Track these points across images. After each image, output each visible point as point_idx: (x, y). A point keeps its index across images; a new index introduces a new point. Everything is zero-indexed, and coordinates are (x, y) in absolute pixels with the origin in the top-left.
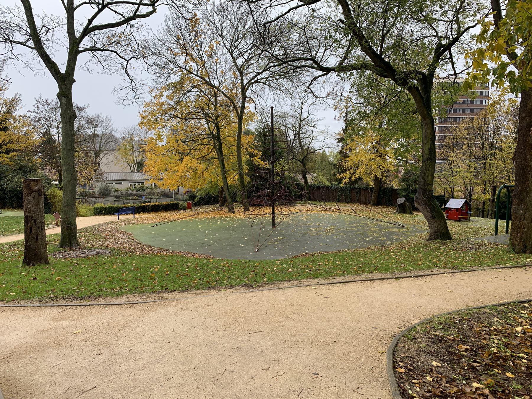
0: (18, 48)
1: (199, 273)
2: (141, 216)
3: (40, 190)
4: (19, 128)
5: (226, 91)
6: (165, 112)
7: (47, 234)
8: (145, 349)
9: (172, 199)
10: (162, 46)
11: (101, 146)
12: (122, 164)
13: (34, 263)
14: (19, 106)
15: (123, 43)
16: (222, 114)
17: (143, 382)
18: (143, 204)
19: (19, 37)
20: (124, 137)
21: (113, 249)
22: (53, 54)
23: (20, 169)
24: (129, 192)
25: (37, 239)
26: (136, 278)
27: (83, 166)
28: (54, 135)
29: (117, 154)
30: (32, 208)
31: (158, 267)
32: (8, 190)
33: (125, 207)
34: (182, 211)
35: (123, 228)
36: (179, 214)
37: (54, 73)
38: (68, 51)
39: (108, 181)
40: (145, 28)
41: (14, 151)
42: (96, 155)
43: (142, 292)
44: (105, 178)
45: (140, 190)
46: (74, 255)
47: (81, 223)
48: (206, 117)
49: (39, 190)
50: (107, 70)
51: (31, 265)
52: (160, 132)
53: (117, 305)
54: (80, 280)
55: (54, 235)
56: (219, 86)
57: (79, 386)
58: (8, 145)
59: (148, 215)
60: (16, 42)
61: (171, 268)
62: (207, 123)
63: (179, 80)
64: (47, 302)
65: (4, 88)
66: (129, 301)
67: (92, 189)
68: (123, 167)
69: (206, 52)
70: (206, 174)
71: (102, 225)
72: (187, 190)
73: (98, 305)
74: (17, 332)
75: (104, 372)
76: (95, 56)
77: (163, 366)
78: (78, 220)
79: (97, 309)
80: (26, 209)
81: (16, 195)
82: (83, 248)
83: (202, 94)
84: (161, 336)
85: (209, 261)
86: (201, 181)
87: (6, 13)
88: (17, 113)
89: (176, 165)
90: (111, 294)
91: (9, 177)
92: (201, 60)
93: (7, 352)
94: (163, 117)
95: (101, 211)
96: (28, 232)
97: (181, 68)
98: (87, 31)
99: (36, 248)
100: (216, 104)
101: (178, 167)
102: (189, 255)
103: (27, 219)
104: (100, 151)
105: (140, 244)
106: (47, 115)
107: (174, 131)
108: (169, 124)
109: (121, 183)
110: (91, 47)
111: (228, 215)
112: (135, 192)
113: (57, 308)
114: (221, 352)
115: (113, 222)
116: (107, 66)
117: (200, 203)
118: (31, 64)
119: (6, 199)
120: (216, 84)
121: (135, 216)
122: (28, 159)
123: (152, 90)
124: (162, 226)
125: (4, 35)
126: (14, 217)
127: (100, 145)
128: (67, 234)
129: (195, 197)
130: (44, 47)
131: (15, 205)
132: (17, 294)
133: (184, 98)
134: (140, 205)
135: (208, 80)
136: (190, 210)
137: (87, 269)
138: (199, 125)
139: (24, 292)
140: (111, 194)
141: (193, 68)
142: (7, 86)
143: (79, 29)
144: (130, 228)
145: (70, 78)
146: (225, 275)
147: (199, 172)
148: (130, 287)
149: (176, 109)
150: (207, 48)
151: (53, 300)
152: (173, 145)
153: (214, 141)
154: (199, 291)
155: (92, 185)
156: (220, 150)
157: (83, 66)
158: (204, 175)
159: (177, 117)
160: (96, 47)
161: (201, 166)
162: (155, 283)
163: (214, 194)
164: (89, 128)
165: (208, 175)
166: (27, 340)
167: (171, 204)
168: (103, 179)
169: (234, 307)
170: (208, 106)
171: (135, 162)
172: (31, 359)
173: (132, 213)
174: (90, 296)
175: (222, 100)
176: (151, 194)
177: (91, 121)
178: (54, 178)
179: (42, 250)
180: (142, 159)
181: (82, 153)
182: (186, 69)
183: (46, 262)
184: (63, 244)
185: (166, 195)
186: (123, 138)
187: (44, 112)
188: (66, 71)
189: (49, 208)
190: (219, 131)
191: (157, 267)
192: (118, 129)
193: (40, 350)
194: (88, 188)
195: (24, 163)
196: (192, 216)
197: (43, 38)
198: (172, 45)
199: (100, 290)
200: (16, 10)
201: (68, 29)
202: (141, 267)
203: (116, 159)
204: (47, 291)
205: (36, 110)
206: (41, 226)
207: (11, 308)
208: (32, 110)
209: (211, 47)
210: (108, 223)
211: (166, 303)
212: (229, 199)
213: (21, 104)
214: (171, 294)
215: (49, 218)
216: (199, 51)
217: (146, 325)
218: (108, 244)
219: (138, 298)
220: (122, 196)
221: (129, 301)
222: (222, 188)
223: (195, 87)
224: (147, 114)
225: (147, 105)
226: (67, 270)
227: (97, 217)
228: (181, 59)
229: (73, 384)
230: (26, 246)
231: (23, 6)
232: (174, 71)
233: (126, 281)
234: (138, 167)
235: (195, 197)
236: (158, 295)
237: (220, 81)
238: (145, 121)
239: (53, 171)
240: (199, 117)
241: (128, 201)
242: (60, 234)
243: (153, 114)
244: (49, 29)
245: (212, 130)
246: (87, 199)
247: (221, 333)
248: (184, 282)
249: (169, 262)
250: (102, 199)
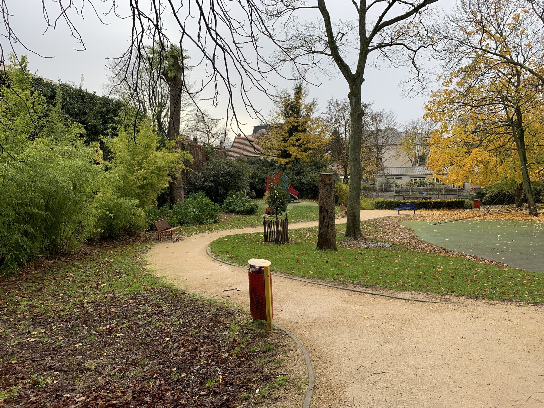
0: (318, 56)
1: (491, 281)
2: (422, 213)
3: (332, 184)
4: (314, 129)
5: (533, 68)
6: (453, 102)
8: (432, 350)
9: (456, 196)
10: (455, 27)
11: (384, 141)
12: (404, 158)
13: (326, 248)
14: (316, 109)
15: (412, 33)
16: (526, 95)
17: (431, 382)
18: (424, 200)
19: (320, 47)
20: (406, 131)
21: (394, 244)
22: (346, 57)
23: (314, 165)
24: (409, 187)
25: (328, 227)
26: (418, 276)
27: (366, 162)
28: (341, 134)
29: (399, 148)
30: (325, 200)
31: (442, 267)
32: (305, 183)
33: (405, 202)
34: (468, 210)
35: (403, 223)
36: (463, 214)
37: (346, 75)
38: (359, 51)
39: (390, 175)
40: (435, 12)
41: (310, 149)
42: (378, 151)
43: (426, 291)
44: (386, 173)
45: (421, 185)
46: (358, 245)
47: (365, 215)
48: (503, 102)
49: (331, 184)
50: (394, 64)
51: (323, 249)
52: (446, 124)
53: (401, 299)
54: (365, 269)
55: (340, 224)
56: (524, 62)
57: (369, 367)
58: (307, 145)
59: (429, 212)
60: (317, 52)
61: (456, 271)
62: (505, 108)
63: (471, 62)
64: (338, 284)
65: (305, 95)
66: (413, 298)
67: (373, 184)
68: (404, 162)
69: (509, 24)
70: (499, 169)
71: (383, 219)
72: (476, 187)
73: (383, 296)
74: (316, 306)
75: (391, 361)
76: (383, 52)
77: (452, 371)
78: (361, 212)
79: (383, 300)
80: (320, 200)
81: (310, 188)
82: (365, 239)
83: (500, 74)
84: (449, 340)
85: (502, 269)
86: (493, 176)
87: (310, 27)
88: (313, 116)
89: (463, 158)
90: (395, 288)
91: (306, 172)
92: (501, 35)
93: (310, 321)
94: (451, 106)
95: (382, 205)
96: (322, 220)
97: (476, 48)
98: (377, 29)
100: (519, 84)
101: (465, 160)
102: (476, 259)
103: (321, 209)
104: (382, 146)
105: (421, 241)
106: (337, 115)
107: (462, 121)
108: (458, 113)
109: (402, 178)
110: (380, 44)
111: (528, 218)
112: (415, 188)
113: (347, 291)
114: (523, 376)
115: (393, 217)
117: (490, 202)
118: (327, 70)
119: (303, 191)
120: (521, 60)
121: (416, 212)
122: (321, 156)
123: (440, 78)
124: (444, 224)
125: (308, 47)
126: (308, 206)
127: (383, 140)
129: (483, 195)
130: (339, 51)
131: (310, 196)
132: (314, 273)
133: (477, 83)
134: (421, 201)
135: (509, 58)
136: (477, 209)
137: (370, 260)
138: (494, 111)
139: (320, 272)
140: (392, 189)
141: (490, 46)
142: (307, 93)
143: (369, 28)
144: (411, 224)
145: (360, 78)
146: (525, 289)
147: (491, 166)
148: (413, 283)
149: (466, 96)
150: (510, 19)
151: (343, 283)
152: (460, 137)
153: (513, 129)
154: (493, 301)
155: (374, 180)
156: (521, 139)
158: (497, 170)
159: (467, 105)
160: (385, 43)
161: (494, 159)
162: (439, 283)
163: (508, 192)
164: (373, 124)
165: (503, 169)
166: (324, 315)
167: (455, 201)
168: (384, 174)
169: (541, 328)
170: (508, 88)
171: (417, 156)
172: (329, 332)
173: (413, 209)
174: (375, 286)
175: (527, 79)
176: (432, 190)
177: (376, 118)
178: (341, 173)
179: (332, 237)
180: (424, 153)
181: (366, 148)
182: (481, 49)
183: (335, 249)
184: (348, 234)
185: (449, 191)
186: (406, 132)
187: (334, 112)
188: (357, 71)
189: (337, 201)
190: (521, 117)
191: (441, 268)
192: (401, 124)
193: (335, 326)
194: (369, 182)
195: (317, 160)
196: (480, 216)
197: (338, 43)
198: (466, 23)
199: (384, 281)
200: (318, 22)
201: (360, 31)
202: (424, 266)
203: (398, 154)
204: (337, 275)
205: (328, 111)
207: (310, 284)
209: (516, 18)
210: (389, 218)
211: (453, 307)
212: (531, 199)
213: (317, 107)
214: (458, 298)
215: (337, 208)
216: (499, 25)
217: (431, 324)
218: (388, 238)
219: (423, 296)
220: (402, 192)
221: (413, 298)
222: (521, 185)
223: (491, 68)
224: (433, 105)
225: (434, 94)
226: (353, 259)
227: (378, 211)
228: (475, 39)
229: (365, 364)
230: (319, 232)
231: (323, 18)
232: (466, 53)
233: (409, 277)
234: (420, 161)
235: (483, 195)
236: (444, 297)
237: (526, 57)
238: (430, 112)
239: (340, 167)
240: (494, 102)
241: (408, 196)
242: (346, 225)
243: (439, 105)
244: (343, 34)
245: (510, 116)
246: (369, 193)
247: (523, 354)
248: (472, 289)
249: (453, 264)
250: (382, 194)
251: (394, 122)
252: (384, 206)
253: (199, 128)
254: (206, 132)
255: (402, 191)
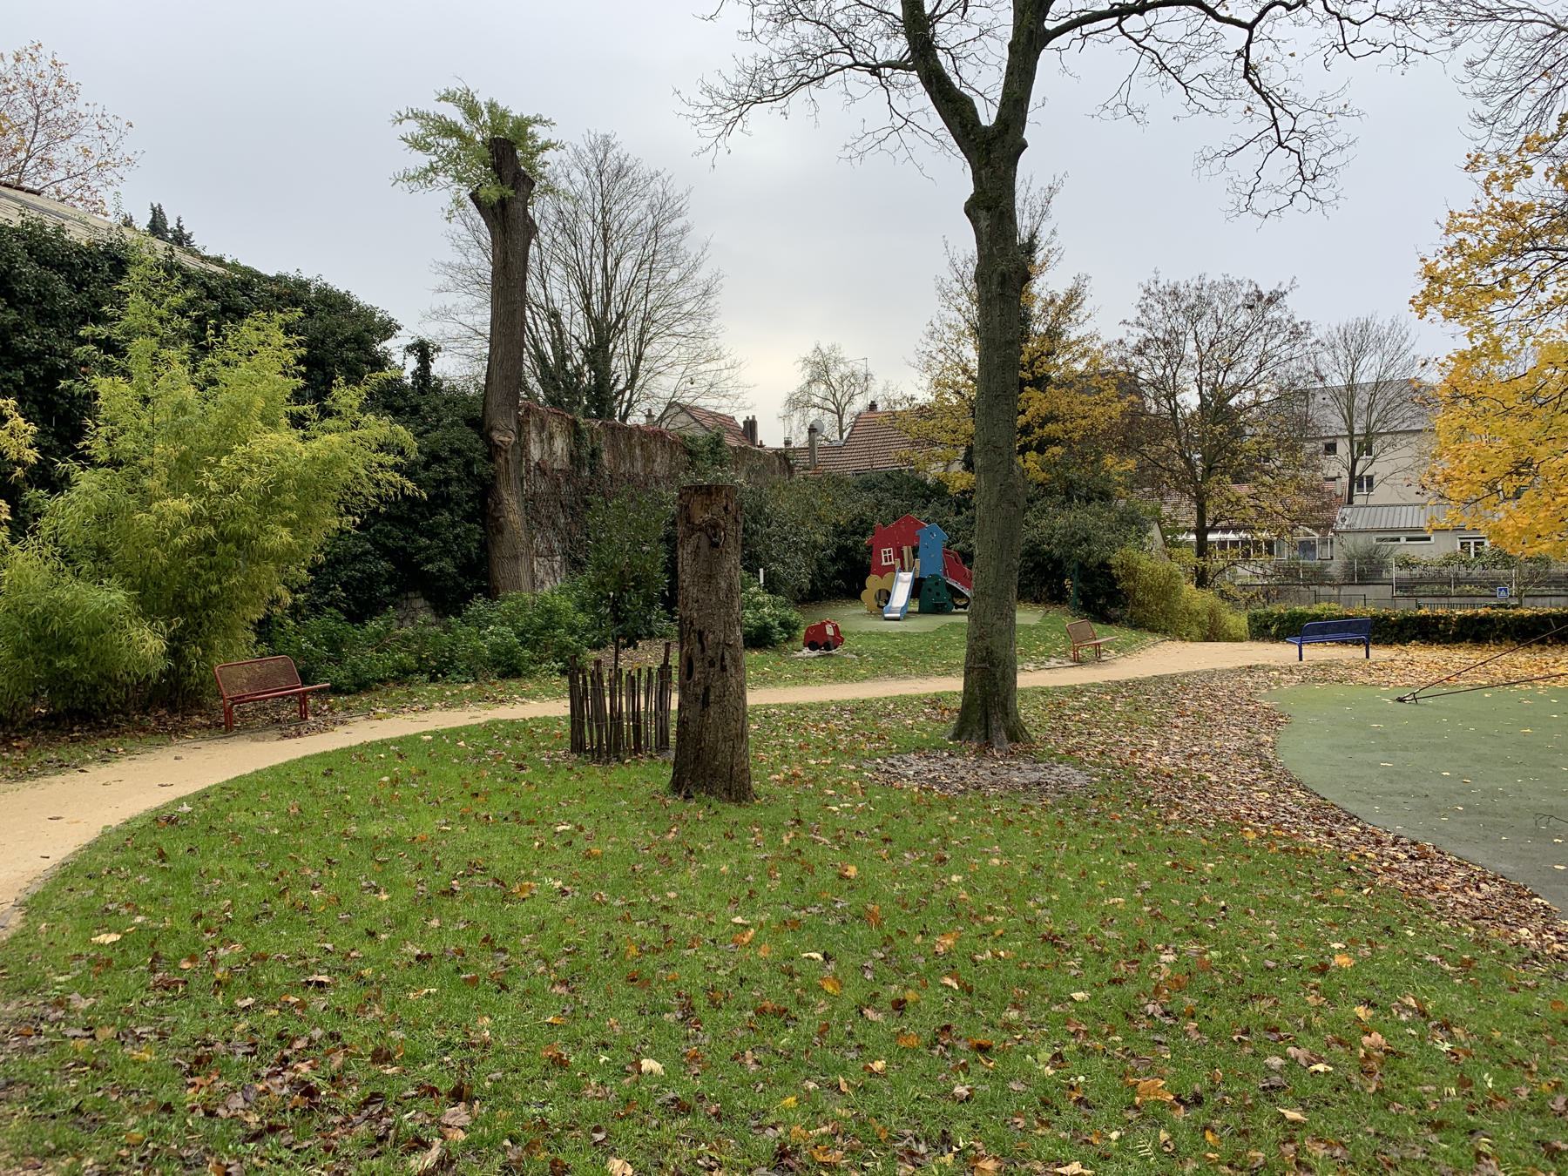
3: (718, 525)
7: (1019, 685)
25: (706, 703)
41: (1053, 441)
50: (1200, 98)
81: (1037, 564)
95: (1267, 627)
99: (700, 733)
112: (1476, 572)
116: (1200, 83)
128: (977, 691)
140: (1385, 575)
145: (1008, 138)
157: (1111, 105)
206: (723, 659)
208: (1132, 320)
213: (1087, 306)
241: (1444, 600)
251: (1409, 356)
252: (1273, 629)
253: (816, 400)
254: (833, 407)
255: (1421, 581)
